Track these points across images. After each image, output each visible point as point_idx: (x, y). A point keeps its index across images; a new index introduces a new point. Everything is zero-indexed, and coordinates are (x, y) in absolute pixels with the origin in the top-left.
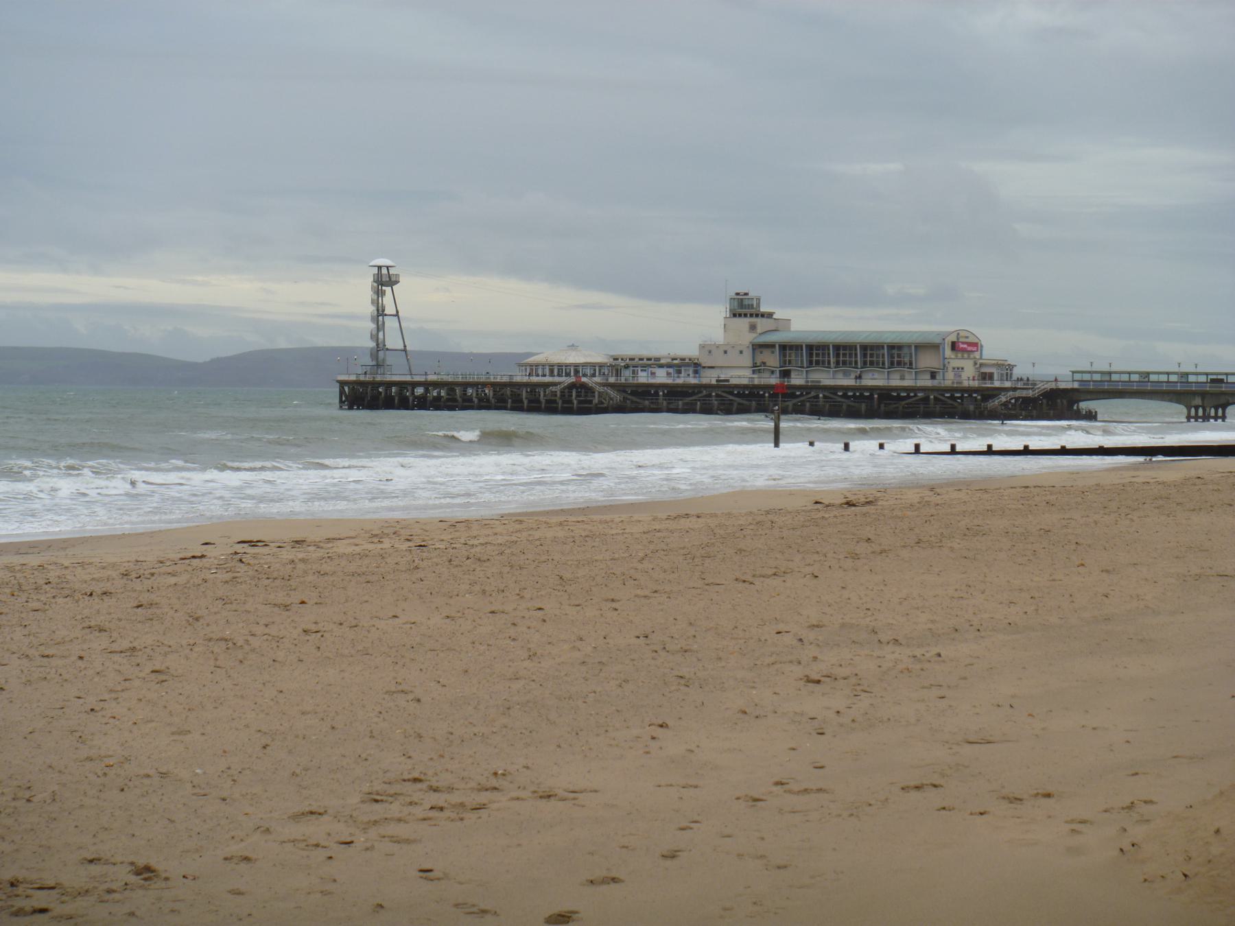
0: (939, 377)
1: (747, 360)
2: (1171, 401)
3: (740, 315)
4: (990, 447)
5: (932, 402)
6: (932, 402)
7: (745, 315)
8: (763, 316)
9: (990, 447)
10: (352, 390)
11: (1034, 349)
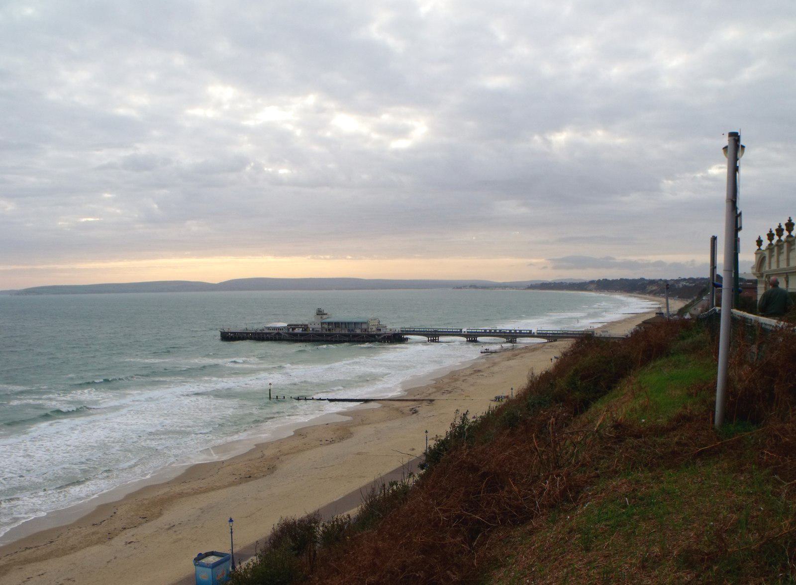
11: (393, 326)
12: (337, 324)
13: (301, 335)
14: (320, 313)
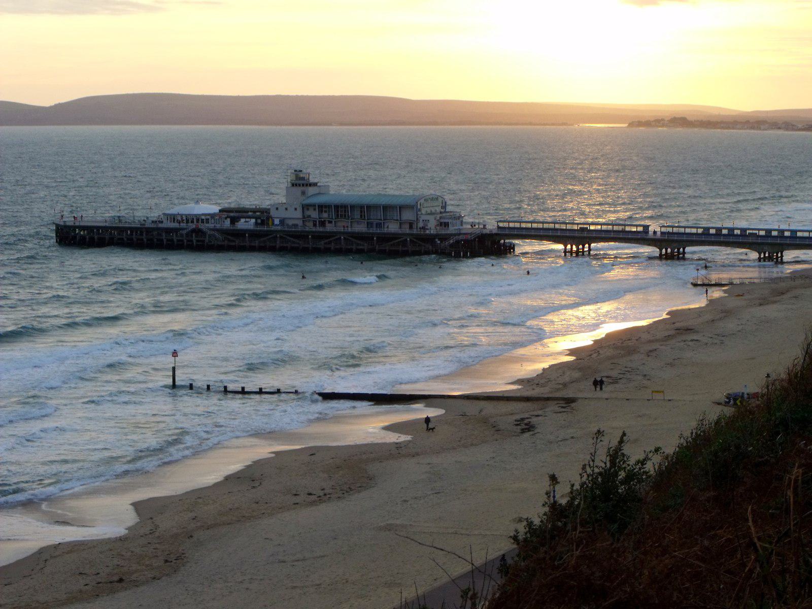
0: (414, 226)
1: (299, 214)
2: (92, 541)
3: (296, 185)
4: (243, 388)
5: (409, 242)
6: (409, 242)
7: (300, 185)
8: (310, 185)
9: (243, 388)
10: (62, 229)
11: (478, 215)
12: (342, 210)
13: (253, 234)
14: (300, 182)
